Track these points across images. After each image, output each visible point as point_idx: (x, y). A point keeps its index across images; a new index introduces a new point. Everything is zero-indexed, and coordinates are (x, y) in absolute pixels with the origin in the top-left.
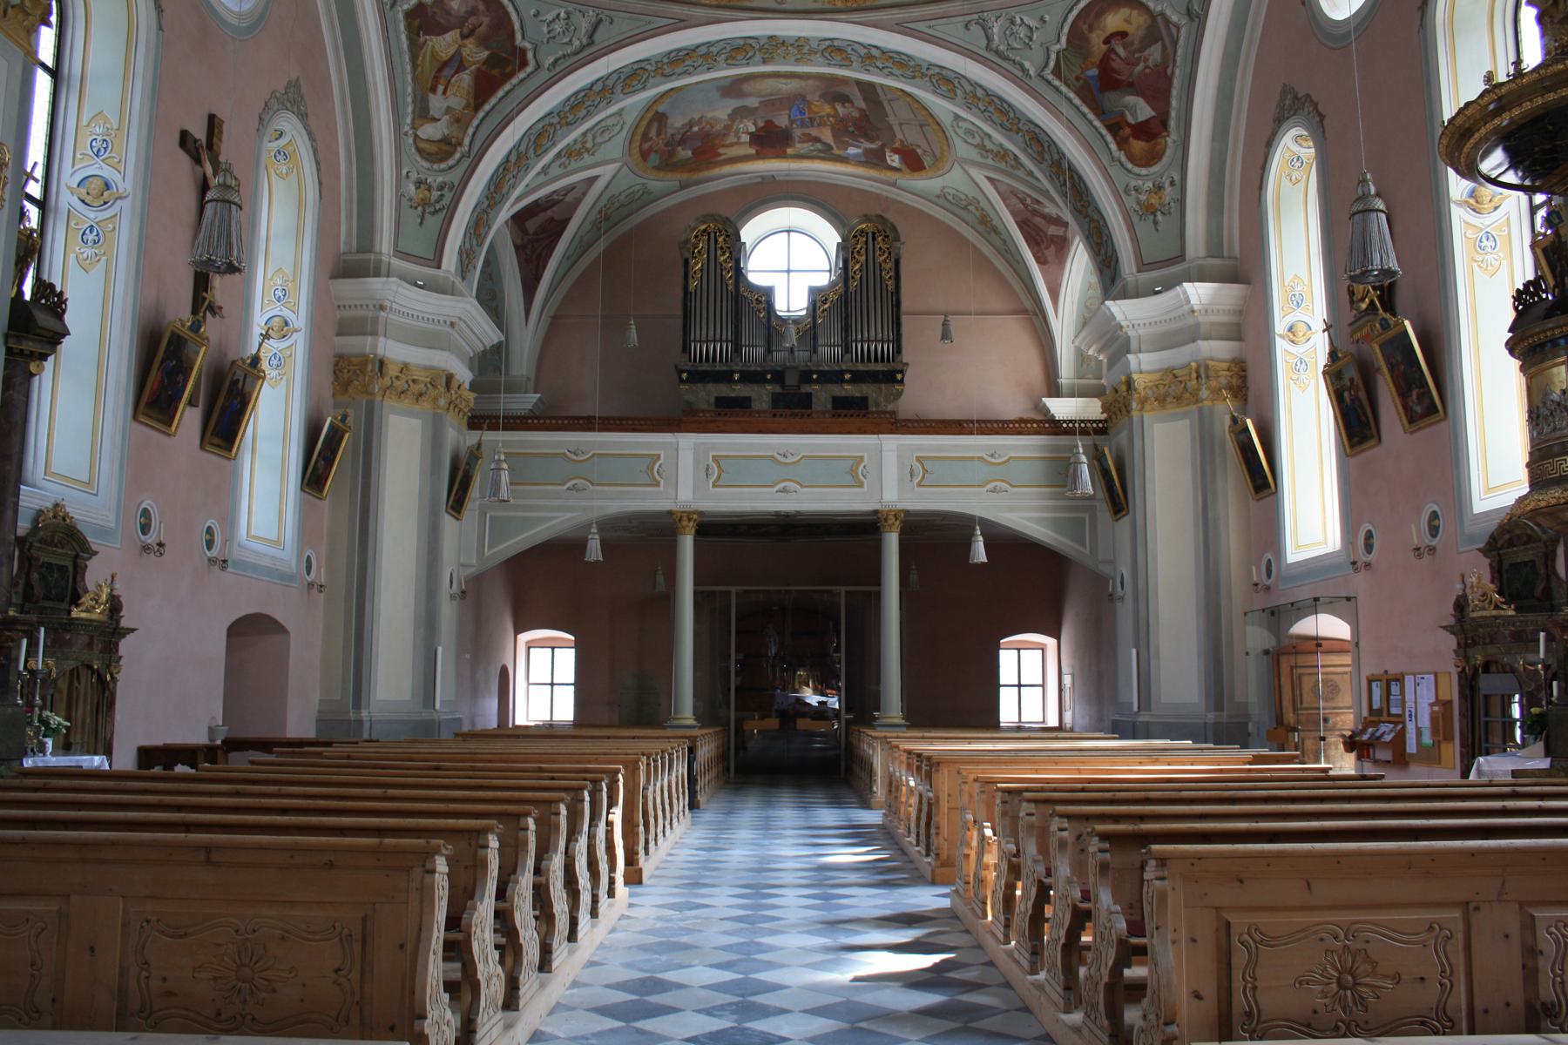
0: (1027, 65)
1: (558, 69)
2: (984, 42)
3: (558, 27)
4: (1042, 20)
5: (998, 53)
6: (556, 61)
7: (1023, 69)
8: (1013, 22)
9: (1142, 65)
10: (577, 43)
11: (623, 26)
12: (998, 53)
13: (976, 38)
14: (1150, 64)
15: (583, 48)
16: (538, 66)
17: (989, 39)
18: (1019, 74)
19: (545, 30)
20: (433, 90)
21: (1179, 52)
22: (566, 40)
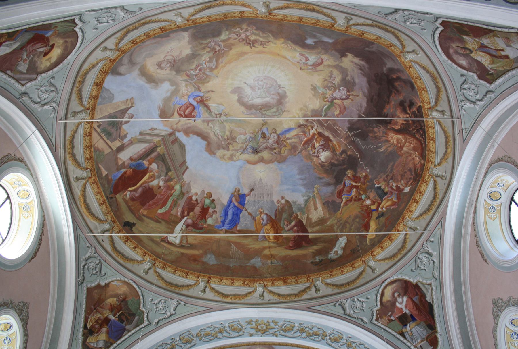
0: (365, 319)
1: (159, 325)
2: (343, 312)
3: (160, 306)
4: (367, 298)
5: (349, 315)
6: (158, 322)
7: (362, 320)
8: (353, 300)
9: (25, 57)
10: (169, 314)
11: (255, 237)
12: (349, 315)
13: (339, 311)
14: (22, 62)
15: (171, 315)
16: (150, 324)
17: (344, 310)
18: (362, 323)
19: (155, 308)
20: (507, 57)
21: (13, 81)
22: (164, 312)
